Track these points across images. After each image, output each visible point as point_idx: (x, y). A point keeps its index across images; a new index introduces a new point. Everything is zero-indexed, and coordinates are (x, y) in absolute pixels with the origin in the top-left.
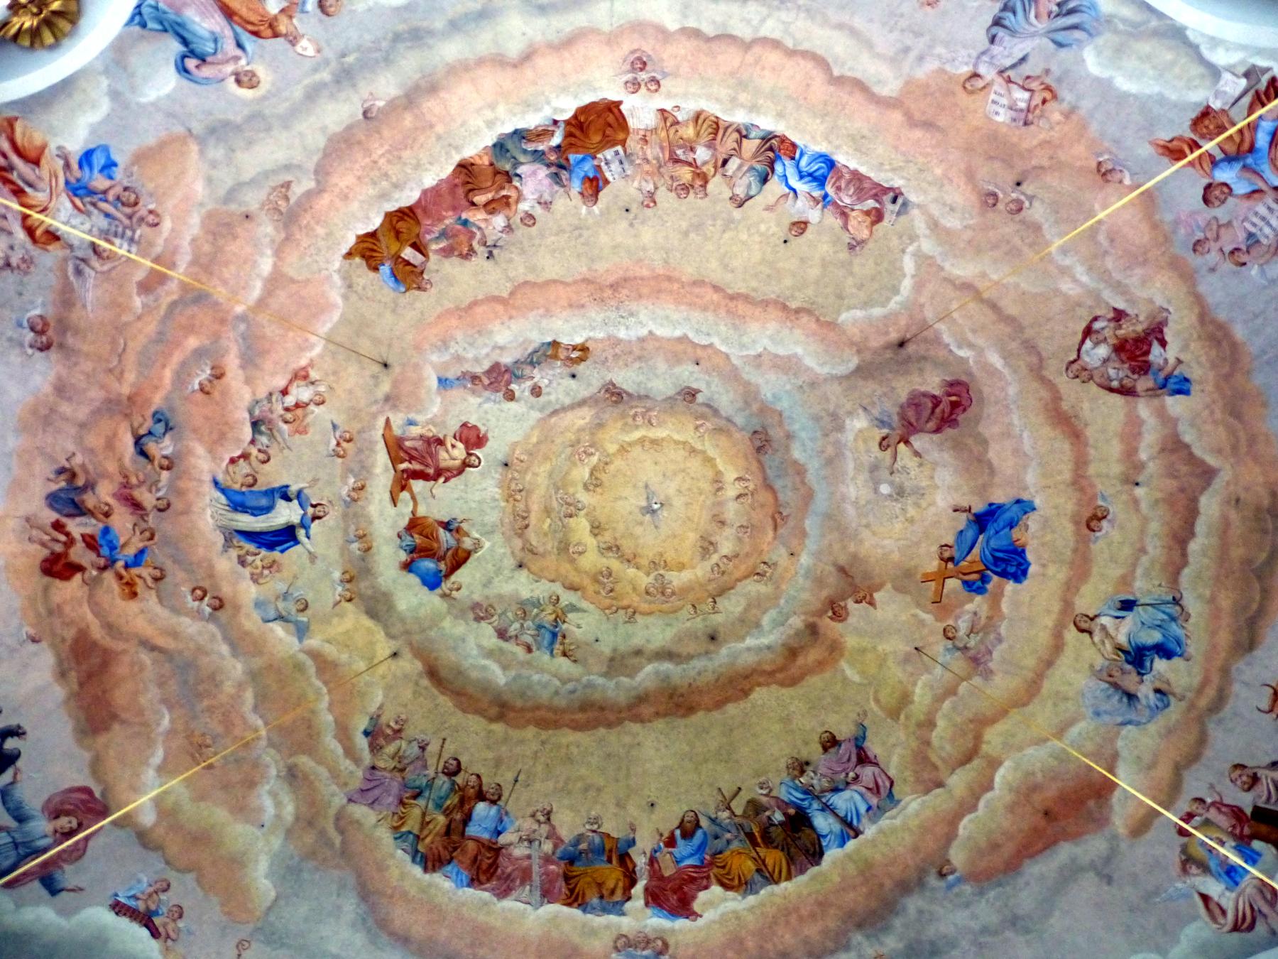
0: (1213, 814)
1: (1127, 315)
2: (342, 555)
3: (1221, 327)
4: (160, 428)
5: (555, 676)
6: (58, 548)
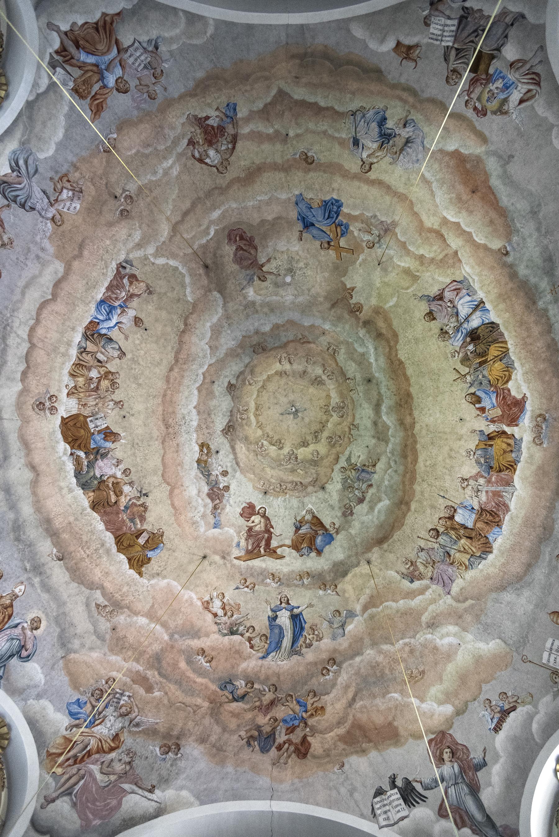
0: (474, 96)
1: (191, 138)
2: (310, 589)
3: (197, 86)
4: (230, 687)
5: (386, 472)
6: (292, 748)
